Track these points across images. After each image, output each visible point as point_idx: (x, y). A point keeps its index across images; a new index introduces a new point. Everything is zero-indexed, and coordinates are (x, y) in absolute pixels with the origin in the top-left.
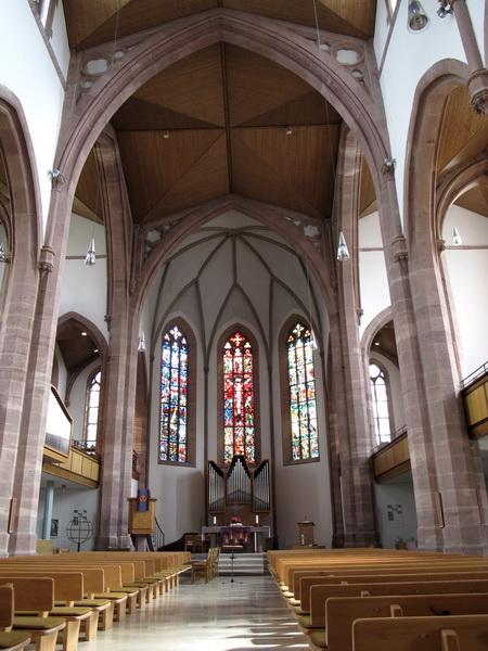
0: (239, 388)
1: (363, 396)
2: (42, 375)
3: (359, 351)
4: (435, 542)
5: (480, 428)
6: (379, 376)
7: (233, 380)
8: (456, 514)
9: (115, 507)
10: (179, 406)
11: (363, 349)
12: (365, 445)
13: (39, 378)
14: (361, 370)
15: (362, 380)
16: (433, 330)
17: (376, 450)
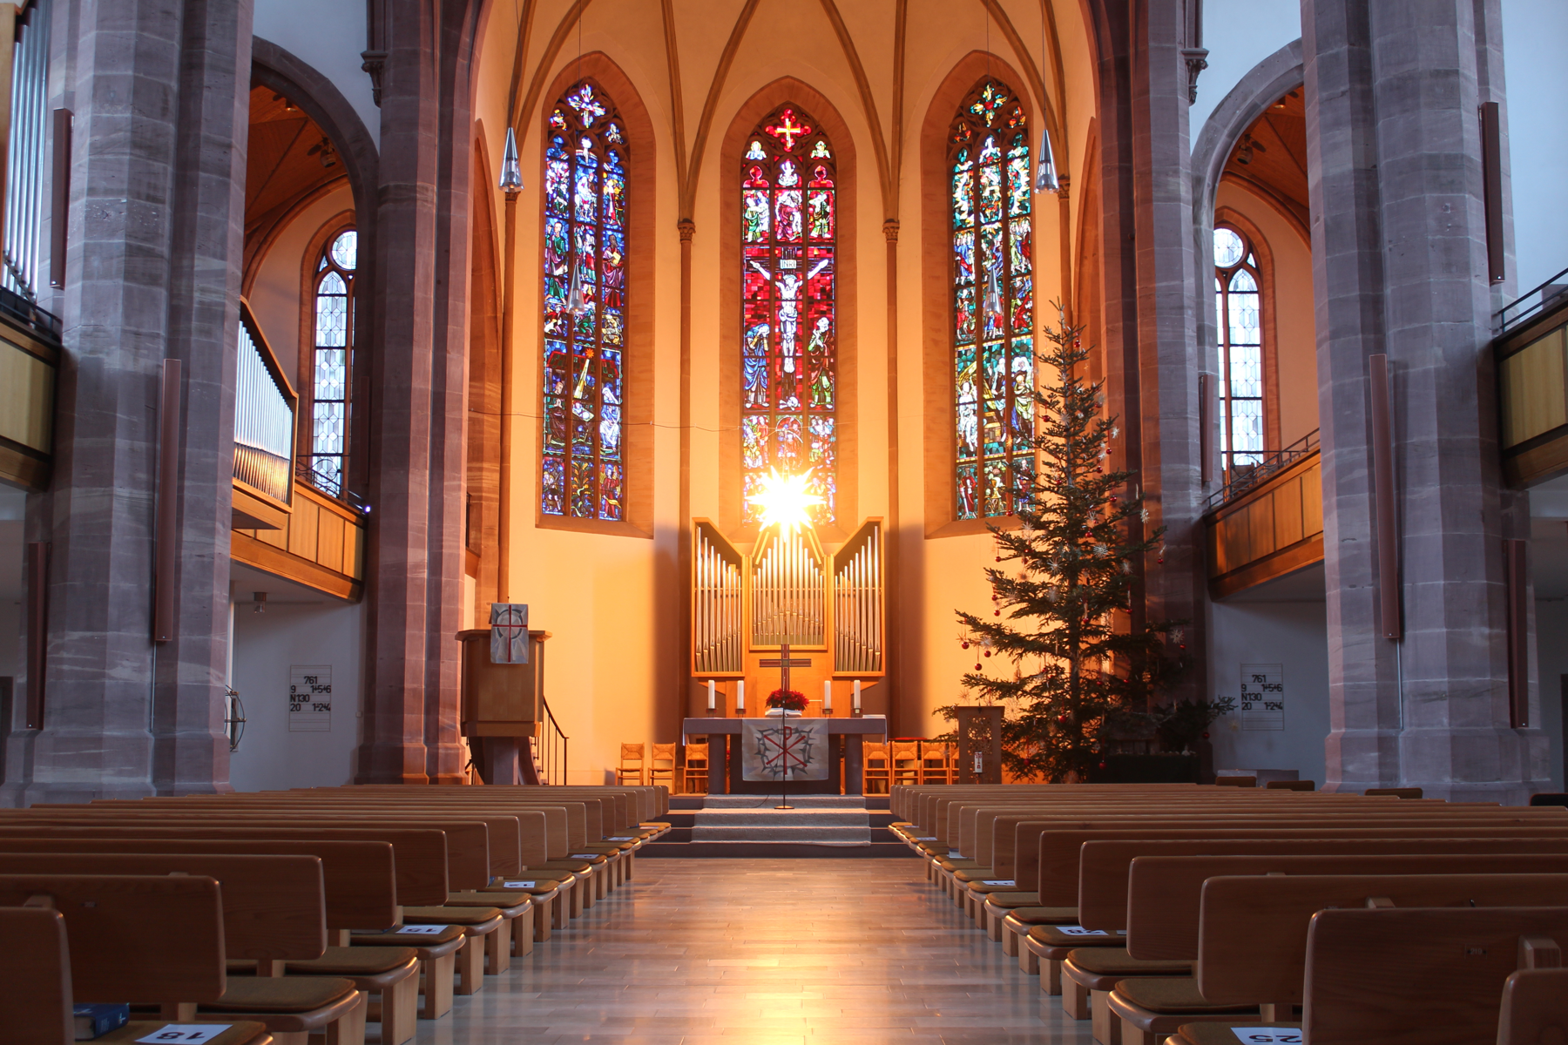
0: (789, 289)
1: (1190, 331)
2: (216, 264)
3: (1184, 189)
4: (1374, 771)
5: (1534, 454)
6: (1242, 264)
7: (772, 265)
8: (1439, 696)
9: (416, 657)
10: (599, 344)
11: (1197, 182)
12: (1185, 484)
13: (207, 274)
14: (1188, 251)
15: (1189, 282)
16: (1426, 150)
17: (1217, 500)
